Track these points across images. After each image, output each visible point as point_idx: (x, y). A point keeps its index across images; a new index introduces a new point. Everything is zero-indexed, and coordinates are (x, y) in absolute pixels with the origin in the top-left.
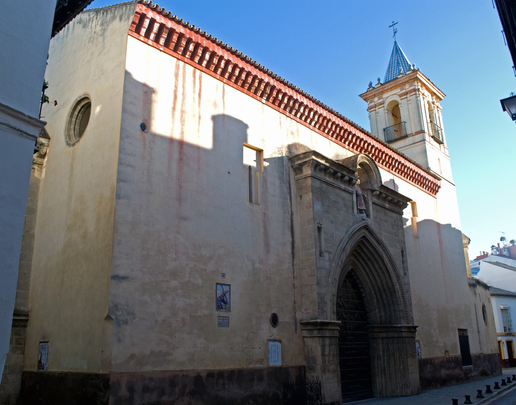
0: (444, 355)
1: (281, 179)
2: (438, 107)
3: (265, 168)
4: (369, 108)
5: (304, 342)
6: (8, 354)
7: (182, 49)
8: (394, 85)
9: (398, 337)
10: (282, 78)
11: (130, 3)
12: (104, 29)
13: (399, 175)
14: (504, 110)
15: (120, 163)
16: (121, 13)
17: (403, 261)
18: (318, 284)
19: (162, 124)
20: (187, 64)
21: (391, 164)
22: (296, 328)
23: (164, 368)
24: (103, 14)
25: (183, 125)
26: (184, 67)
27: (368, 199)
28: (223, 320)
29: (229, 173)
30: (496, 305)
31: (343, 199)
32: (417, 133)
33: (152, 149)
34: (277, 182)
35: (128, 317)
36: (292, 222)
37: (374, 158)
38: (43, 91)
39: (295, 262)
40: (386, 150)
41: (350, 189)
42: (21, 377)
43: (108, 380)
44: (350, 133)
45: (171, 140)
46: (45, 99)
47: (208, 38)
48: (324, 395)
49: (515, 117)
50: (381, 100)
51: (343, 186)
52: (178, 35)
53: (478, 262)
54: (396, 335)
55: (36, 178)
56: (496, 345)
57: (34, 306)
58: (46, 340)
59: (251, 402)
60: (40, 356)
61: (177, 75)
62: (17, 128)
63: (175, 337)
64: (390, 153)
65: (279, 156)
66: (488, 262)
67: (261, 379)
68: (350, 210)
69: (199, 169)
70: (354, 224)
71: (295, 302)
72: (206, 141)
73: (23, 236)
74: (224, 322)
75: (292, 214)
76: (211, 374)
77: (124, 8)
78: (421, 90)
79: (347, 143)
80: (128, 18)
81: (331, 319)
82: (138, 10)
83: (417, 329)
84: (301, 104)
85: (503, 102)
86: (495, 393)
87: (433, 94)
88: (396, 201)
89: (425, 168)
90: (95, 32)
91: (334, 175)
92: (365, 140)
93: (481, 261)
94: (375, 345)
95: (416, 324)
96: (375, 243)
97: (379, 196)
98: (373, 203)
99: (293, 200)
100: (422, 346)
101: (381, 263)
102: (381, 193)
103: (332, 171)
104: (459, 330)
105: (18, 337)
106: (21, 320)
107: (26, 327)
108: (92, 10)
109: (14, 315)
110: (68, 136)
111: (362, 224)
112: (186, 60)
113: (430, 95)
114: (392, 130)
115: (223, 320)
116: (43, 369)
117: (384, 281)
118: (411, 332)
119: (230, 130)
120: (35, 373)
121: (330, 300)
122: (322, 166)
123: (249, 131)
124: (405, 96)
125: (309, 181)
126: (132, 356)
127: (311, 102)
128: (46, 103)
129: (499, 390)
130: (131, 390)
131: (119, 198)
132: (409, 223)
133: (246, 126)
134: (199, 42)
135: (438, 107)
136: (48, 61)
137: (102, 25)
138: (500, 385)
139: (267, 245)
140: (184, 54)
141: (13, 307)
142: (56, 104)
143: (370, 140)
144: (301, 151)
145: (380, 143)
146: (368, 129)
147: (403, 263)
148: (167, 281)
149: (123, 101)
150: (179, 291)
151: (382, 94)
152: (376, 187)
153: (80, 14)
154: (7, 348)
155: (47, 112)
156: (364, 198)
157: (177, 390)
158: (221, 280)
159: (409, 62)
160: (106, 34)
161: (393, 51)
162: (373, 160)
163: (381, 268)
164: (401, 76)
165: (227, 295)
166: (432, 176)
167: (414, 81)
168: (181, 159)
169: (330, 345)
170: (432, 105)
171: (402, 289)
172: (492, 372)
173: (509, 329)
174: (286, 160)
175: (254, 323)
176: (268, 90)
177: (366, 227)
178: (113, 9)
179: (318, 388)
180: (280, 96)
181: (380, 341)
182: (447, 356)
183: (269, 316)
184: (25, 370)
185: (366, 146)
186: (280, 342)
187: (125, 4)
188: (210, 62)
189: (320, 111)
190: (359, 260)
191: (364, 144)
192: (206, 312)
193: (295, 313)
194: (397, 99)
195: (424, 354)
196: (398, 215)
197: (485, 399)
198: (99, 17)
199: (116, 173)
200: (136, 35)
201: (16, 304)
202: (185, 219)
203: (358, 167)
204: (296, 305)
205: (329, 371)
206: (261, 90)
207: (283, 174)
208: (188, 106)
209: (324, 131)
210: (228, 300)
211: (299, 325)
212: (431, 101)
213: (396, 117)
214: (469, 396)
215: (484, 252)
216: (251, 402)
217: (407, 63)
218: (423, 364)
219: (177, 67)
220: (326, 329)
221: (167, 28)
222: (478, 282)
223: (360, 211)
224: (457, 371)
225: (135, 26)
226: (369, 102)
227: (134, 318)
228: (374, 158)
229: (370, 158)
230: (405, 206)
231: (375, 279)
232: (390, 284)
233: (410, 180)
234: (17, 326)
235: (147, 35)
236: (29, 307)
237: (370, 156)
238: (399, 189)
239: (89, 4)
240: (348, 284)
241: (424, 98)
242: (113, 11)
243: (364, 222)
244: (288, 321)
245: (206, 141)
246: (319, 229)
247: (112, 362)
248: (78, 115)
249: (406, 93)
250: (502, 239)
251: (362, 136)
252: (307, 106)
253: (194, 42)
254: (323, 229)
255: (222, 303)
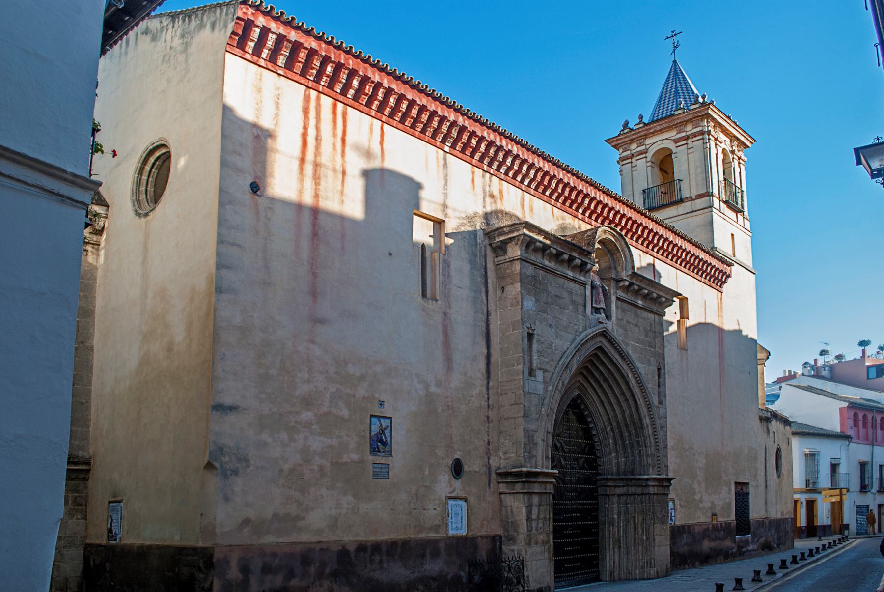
0: (710, 520)
1: (472, 263)
2: (739, 158)
3: (447, 246)
4: (622, 159)
5: (501, 501)
6: (62, 520)
7: (315, 72)
8: (666, 125)
9: (642, 494)
10: (478, 115)
11: (228, 4)
12: (186, 43)
13: (664, 258)
14: (859, 162)
15: (220, 241)
16: (212, 19)
17: (659, 383)
18: (525, 415)
19: (285, 182)
20: (322, 96)
21: (650, 243)
22: (490, 480)
23: (294, 538)
24: (184, 20)
25: (317, 184)
26: (318, 99)
27: (610, 292)
28: (381, 468)
29: (390, 254)
30: (798, 449)
31: (570, 293)
32: (699, 196)
33: (269, 219)
34: (467, 267)
35: (239, 465)
36: (488, 325)
37: (623, 233)
38: (93, 135)
39: (491, 384)
40: (645, 221)
41: (583, 278)
42: (82, 552)
43: (212, 556)
44: (587, 195)
45: (299, 207)
46: (96, 148)
47: (357, 57)
48: (528, 577)
49: (883, 175)
50: (643, 148)
51: (570, 274)
52: (307, 52)
53: (777, 387)
54: (639, 491)
55: (91, 264)
56: (791, 506)
57: (98, 448)
58: (118, 499)
59: (421, 587)
60: (110, 521)
61: (306, 111)
62: (56, 192)
63: (309, 493)
64: (651, 225)
65: (470, 229)
66: (795, 386)
67: (436, 554)
68: (581, 309)
69: (343, 248)
70: (585, 329)
71: (489, 443)
72: (353, 207)
73: (76, 349)
74: (382, 472)
75: (488, 314)
76: (362, 548)
77: (218, 11)
78: (712, 132)
79: (581, 211)
80: (226, 26)
81: (542, 467)
82: (240, 14)
83: (672, 482)
84: (508, 153)
85: (857, 151)
86: (780, 575)
87: (733, 138)
88: (655, 295)
89: (707, 247)
90: (171, 48)
91: (557, 257)
92: (610, 206)
93: (783, 385)
94: (607, 506)
95: (671, 475)
96: (616, 357)
97: (627, 289)
98: (618, 299)
99: (490, 294)
100: (678, 507)
101: (624, 387)
102: (631, 284)
103: (555, 251)
104: (736, 483)
105: (76, 495)
106: (79, 471)
107: (87, 480)
108: (164, 15)
109: (69, 463)
110: (137, 202)
111: (598, 329)
112: (321, 89)
113: (728, 140)
114: (657, 191)
115: (381, 468)
116: (115, 540)
117: (627, 413)
118: (662, 486)
119: (390, 191)
120: (104, 546)
121: (543, 440)
122: (538, 244)
123: (424, 194)
124: (685, 142)
125: (517, 266)
126: (246, 522)
127: (524, 149)
128: (100, 153)
129: (786, 571)
130: (245, 570)
131: (221, 292)
132: (673, 328)
133: (419, 186)
134: (342, 61)
135: (739, 158)
136: (97, 91)
137: (183, 36)
138: (788, 563)
139: (448, 359)
140: (317, 79)
141: (67, 452)
142: (115, 155)
143: (618, 207)
144: (506, 222)
145: (635, 210)
146: (617, 190)
147: (659, 386)
148: (297, 413)
149: (222, 149)
150: (314, 427)
151: (645, 139)
152: (624, 275)
153: (145, 21)
154: (60, 511)
155: (101, 167)
156: (604, 290)
157: (312, 570)
158: (378, 411)
159: (696, 92)
160: (189, 51)
161: (669, 74)
162: (621, 236)
163: (623, 393)
164: (680, 112)
165: (387, 432)
166: (717, 259)
167: (702, 120)
168: (315, 235)
169: (540, 505)
170: (731, 156)
171: (653, 424)
172: (778, 545)
173: (814, 483)
174: (480, 234)
175: (426, 473)
176: (454, 133)
177: (605, 334)
178: (200, 13)
179: (519, 568)
180: (474, 142)
181: (615, 499)
182: (714, 522)
183: (450, 462)
184: (88, 541)
185: (611, 216)
186: (465, 500)
187: (220, 6)
188: (360, 91)
189: (539, 163)
190: (589, 382)
191: (609, 212)
192: (355, 457)
193: (489, 459)
194: (671, 145)
195: (679, 517)
196: (656, 317)
197: (764, 584)
198: (176, 25)
199: (215, 256)
200: (238, 51)
201: (71, 447)
202: (322, 321)
203: (597, 245)
204: (490, 447)
205: (536, 544)
206: (442, 132)
207: (476, 256)
208: (324, 153)
209: (543, 193)
210: (389, 440)
211: (494, 475)
212: (728, 149)
213: (666, 172)
214: (741, 580)
215: (790, 372)
216: (421, 587)
217: (693, 93)
218: (677, 532)
219: (307, 99)
220: (535, 482)
221: (289, 41)
222: (775, 415)
223: (597, 310)
224: (728, 543)
225: (237, 38)
226: (621, 150)
227: (248, 466)
228: (623, 233)
229: (617, 232)
230: (670, 303)
231: (614, 410)
232: (636, 417)
233: (680, 265)
234: (73, 479)
235: (257, 52)
236: (91, 451)
237: (618, 229)
238: (662, 279)
239: (160, 4)
240: (572, 416)
241: (716, 145)
242: (200, 15)
243: (601, 326)
244: (478, 469)
245: (353, 207)
246: (530, 336)
247: (217, 530)
248: (150, 171)
249: (687, 138)
250: (823, 353)
251: (606, 200)
252: (518, 155)
253: (334, 62)
254: (536, 336)
255: (379, 443)
